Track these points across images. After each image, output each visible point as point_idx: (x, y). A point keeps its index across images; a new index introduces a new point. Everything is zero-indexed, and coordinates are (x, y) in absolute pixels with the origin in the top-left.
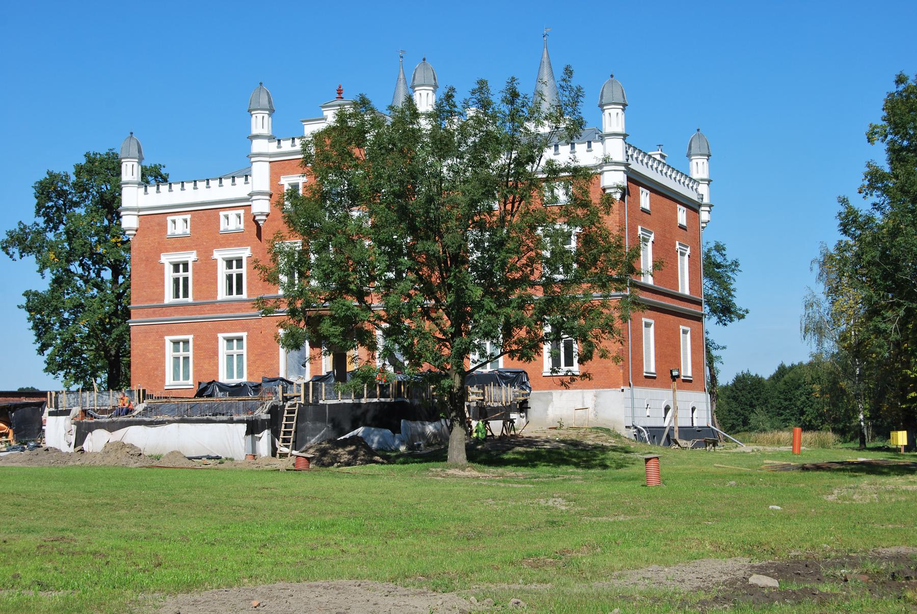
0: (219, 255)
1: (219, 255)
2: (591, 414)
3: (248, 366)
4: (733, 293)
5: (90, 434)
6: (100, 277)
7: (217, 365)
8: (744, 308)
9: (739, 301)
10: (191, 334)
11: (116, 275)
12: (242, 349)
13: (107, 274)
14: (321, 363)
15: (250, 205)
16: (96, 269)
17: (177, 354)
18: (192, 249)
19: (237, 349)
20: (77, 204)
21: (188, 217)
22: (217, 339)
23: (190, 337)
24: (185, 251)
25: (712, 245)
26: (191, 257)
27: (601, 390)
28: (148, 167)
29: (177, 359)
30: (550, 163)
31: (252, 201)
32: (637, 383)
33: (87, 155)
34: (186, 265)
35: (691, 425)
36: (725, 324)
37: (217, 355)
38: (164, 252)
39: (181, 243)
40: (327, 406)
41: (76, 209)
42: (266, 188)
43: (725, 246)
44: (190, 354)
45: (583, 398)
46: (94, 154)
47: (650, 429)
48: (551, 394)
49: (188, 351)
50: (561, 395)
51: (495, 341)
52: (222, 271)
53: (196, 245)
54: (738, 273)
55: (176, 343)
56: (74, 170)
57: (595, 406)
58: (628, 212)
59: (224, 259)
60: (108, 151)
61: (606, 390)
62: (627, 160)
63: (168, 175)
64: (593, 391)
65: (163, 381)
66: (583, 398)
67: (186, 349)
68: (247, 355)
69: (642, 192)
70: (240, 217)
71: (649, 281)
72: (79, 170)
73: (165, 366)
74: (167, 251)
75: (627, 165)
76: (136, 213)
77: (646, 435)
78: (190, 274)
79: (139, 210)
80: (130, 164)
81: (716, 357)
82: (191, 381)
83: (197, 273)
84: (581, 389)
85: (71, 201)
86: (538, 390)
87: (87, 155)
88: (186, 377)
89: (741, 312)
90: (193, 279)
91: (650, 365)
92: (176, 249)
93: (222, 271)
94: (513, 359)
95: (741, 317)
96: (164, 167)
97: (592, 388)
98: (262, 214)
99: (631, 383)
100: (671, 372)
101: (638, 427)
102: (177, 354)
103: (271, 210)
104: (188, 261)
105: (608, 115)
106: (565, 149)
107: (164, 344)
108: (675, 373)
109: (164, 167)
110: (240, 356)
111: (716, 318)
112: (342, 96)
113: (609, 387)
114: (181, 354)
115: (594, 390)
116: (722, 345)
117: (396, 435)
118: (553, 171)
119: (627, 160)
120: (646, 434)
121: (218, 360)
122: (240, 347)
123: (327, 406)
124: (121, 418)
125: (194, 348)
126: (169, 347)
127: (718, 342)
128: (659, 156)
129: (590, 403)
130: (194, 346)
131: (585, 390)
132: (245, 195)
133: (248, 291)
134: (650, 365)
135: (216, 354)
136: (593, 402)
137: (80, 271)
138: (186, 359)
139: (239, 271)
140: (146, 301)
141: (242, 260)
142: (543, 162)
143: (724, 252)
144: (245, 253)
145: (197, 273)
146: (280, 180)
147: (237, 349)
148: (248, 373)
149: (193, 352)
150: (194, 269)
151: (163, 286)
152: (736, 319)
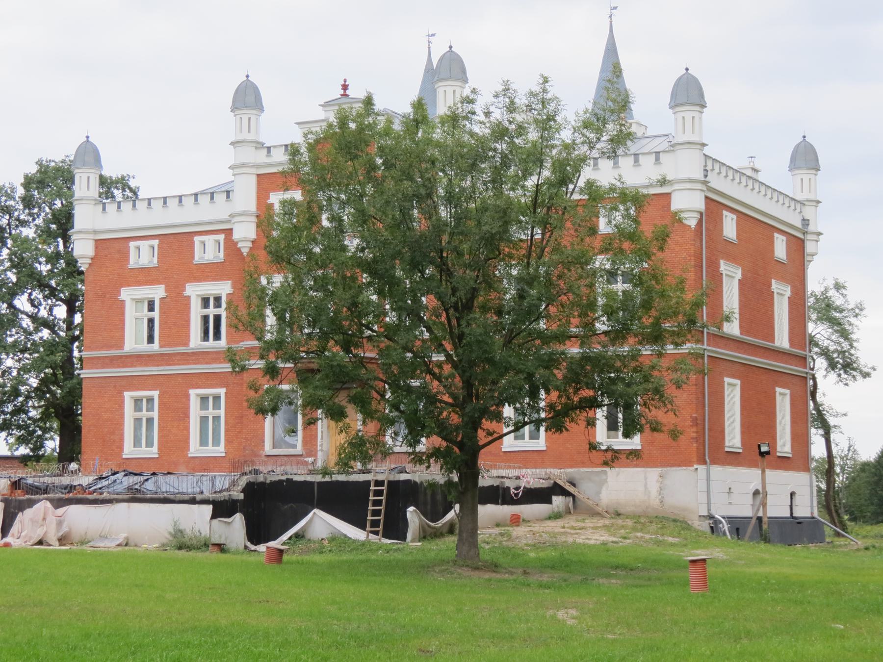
0: (194, 291)
1: (194, 291)
2: (654, 501)
3: (226, 431)
4: (855, 344)
5: (20, 514)
6: (51, 315)
7: (187, 429)
8: (870, 366)
9: (863, 355)
10: (156, 390)
11: (71, 311)
12: (219, 409)
13: (61, 311)
14: (317, 429)
15: (232, 229)
16: (47, 304)
17: (138, 414)
18: (160, 283)
19: (213, 409)
20: (23, 223)
21: (156, 242)
22: (188, 396)
23: (155, 394)
24: (151, 285)
25: (830, 283)
26: (158, 292)
27: (669, 468)
28: (114, 179)
29: (138, 420)
30: (590, 184)
31: (234, 223)
32: (715, 461)
33: (39, 163)
34: (218, 300)
35: (788, 515)
36: (846, 384)
37: (189, 417)
38: (125, 287)
39: (144, 276)
40: (316, 485)
41: (23, 229)
42: (252, 207)
43: (845, 284)
44: (155, 414)
45: (646, 478)
46: (47, 162)
47: (730, 519)
48: (605, 473)
49: (220, 409)
50: (618, 474)
51: (518, 405)
52: (196, 312)
53: (165, 278)
54: (863, 319)
55: (204, 399)
56: (22, 181)
57: (661, 490)
58: (706, 242)
59: (198, 295)
60: (64, 158)
61: (675, 468)
62: (706, 176)
63: (138, 188)
64: (658, 470)
65: (121, 448)
66: (646, 478)
67: (150, 409)
68: (226, 417)
69: (726, 216)
70: (154, 248)
71: (733, 328)
72: (28, 183)
73: (123, 430)
74: (129, 286)
75: (705, 183)
76: (92, 237)
77: (726, 527)
78: (222, 311)
79: (95, 232)
80: (84, 177)
81: (835, 426)
82: (155, 449)
83: (165, 313)
84: (644, 467)
85: (18, 219)
86: (588, 467)
87: (39, 163)
88: (149, 444)
89: (866, 370)
90: (160, 321)
91: (733, 439)
92: (139, 283)
93: (196, 312)
94: (567, 430)
95: (866, 375)
96: (134, 178)
97: (657, 466)
98: (245, 240)
99: (708, 461)
100: (759, 446)
101: (717, 516)
102: (138, 414)
103: (257, 235)
104: (154, 298)
105: (681, 118)
106: (605, 164)
107: (123, 402)
108: (764, 449)
109: (134, 178)
110: (216, 418)
111: (835, 376)
112: (348, 92)
113: (679, 466)
114: (144, 414)
115: (659, 469)
116: (843, 413)
117: (238, 520)
118: (594, 192)
119: (706, 176)
120: (725, 526)
121: (189, 422)
122: (150, 409)
123: (316, 485)
124: (833, 508)
125: (159, 408)
126: (129, 405)
127: (838, 408)
128: (750, 170)
129: (654, 487)
130: (160, 405)
131: (649, 469)
132: (225, 216)
133: (227, 336)
134: (733, 439)
135: (187, 415)
136: (658, 485)
137: (28, 308)
138: (150, 421)
139: (217, 311)
140: (102, 348)
141: (154, 301)
142: (581, 183)
143: (844, 292)
144: (224, 288)
145: (165, 313)
146: (269, 198)
147: (213, 409)
148: (225, 440)
149: (159, 412)
150: (161, 309)
151: (123, 329)
152: (859, 377)
